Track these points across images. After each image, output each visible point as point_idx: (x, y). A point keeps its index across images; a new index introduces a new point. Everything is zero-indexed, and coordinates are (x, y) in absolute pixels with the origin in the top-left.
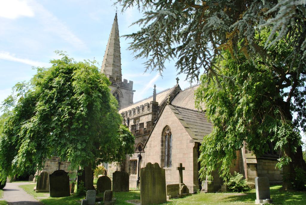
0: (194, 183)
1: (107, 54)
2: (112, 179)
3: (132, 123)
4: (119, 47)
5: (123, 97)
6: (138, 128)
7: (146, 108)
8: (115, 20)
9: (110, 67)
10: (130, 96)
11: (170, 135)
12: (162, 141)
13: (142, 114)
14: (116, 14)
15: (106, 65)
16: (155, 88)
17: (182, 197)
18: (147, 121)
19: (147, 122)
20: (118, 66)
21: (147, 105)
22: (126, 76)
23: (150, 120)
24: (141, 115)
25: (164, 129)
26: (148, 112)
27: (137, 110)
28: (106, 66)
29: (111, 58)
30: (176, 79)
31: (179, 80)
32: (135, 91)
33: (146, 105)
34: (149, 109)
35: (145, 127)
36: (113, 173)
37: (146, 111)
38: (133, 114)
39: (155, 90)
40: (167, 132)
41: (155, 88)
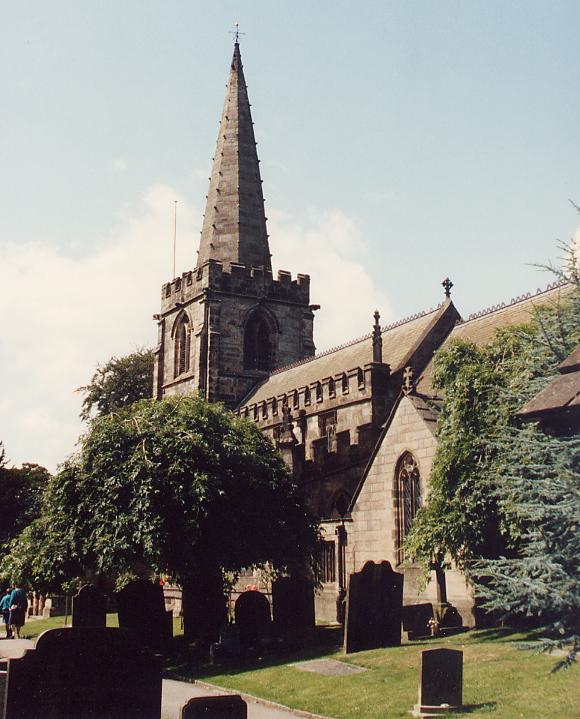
1: (218, 190)
2: (270, 598)
3: (313, 425)
4: (253, 160)
5: (280, 333)
6: (333, 447)
7: (353, 381)
8: (233, 67)
10: (303, 325)
13: (344, 400)
14: (237, 45)
15: (219, 209)
16: (377, 322)
18: (359, 425)
19: (358, 428)
21: (355, 375)
22: (286, 257)
23: (369, 420)
24: (340, 404)
26: (361, 396)
27: (326, 388)
28: (218, 232)
29: (232, 203)
30: (444, 284)
31: (451, 285)
32: (317, 307)
33: (353, 372)
34: (362, 386)
36: (28, 650)
37: (354, 390)
38: (316, 401)
39: (377, 328)
40: (410, 468)
41: (377, 322)
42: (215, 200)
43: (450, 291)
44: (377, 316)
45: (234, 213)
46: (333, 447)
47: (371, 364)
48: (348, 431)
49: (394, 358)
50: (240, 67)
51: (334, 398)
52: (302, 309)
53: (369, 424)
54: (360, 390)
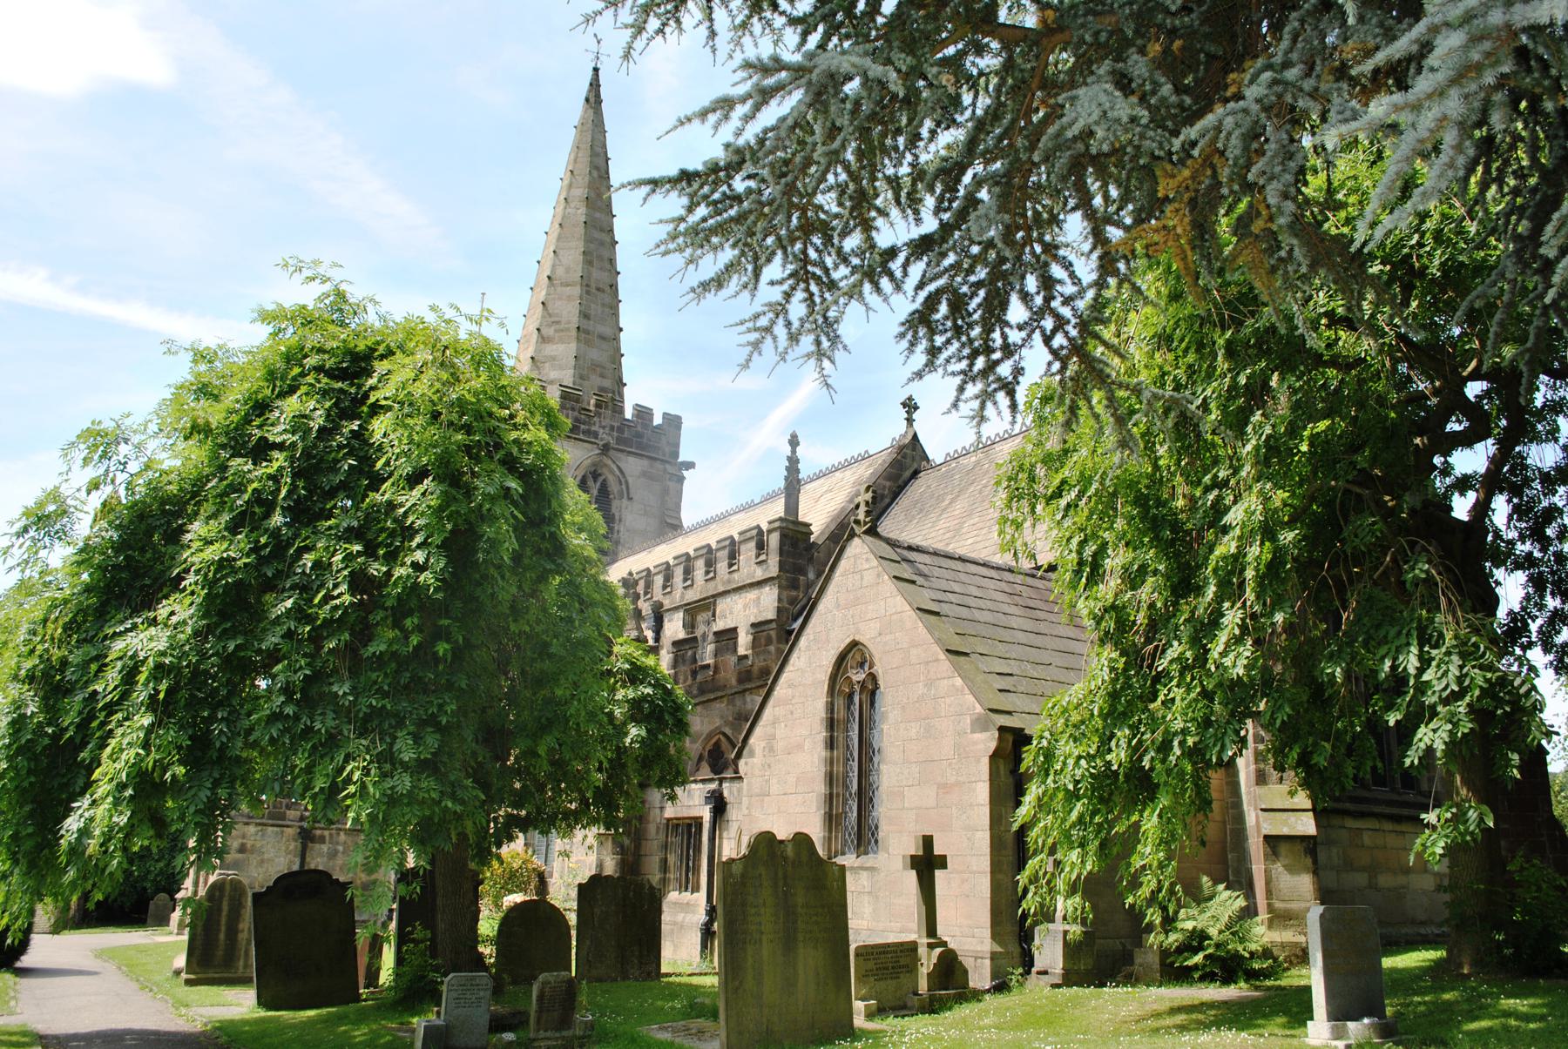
0: (995, 936)
1: (549, 277)
2: (572, 918)
3: (674, 628)
5: (630, 499)
6: (707, 654)
8: (587, 100)
9: (561, 341)
10: (666, 491)
11: (871, 688)
12: (831, 724)
13: (729, 581)
14: (596, 70)
15: (550, 306)
16: (794, 452)
17: (932, 1006)
18: (753, 620)
20: (602, 338)
24: (721, 589)
25: (842, 659)
26: (760, 574)
28: (543, 339)
30: (904, 405)
31: (916, 408)
32: (690, 465)
33: (748, 535)
34: (763, 557)
35: (741, 651)
37: (749, 567)
40: (858, 676)
41: (794, 452)
42: (544, 293)
43: (914, 416)
44: (794, 442)
45: (569, 311)
46: (707, 654)
47: (780, 519)
48: (734, 630)
49: (817, 514)
50: (598, 101)
51: (712, 579)
52: (667, 466)
53: (770, 621)
54: (759, 563)
